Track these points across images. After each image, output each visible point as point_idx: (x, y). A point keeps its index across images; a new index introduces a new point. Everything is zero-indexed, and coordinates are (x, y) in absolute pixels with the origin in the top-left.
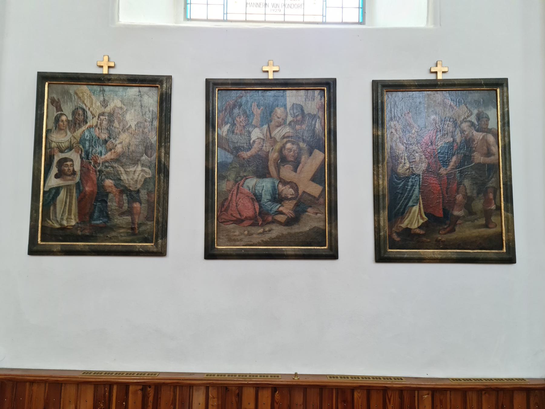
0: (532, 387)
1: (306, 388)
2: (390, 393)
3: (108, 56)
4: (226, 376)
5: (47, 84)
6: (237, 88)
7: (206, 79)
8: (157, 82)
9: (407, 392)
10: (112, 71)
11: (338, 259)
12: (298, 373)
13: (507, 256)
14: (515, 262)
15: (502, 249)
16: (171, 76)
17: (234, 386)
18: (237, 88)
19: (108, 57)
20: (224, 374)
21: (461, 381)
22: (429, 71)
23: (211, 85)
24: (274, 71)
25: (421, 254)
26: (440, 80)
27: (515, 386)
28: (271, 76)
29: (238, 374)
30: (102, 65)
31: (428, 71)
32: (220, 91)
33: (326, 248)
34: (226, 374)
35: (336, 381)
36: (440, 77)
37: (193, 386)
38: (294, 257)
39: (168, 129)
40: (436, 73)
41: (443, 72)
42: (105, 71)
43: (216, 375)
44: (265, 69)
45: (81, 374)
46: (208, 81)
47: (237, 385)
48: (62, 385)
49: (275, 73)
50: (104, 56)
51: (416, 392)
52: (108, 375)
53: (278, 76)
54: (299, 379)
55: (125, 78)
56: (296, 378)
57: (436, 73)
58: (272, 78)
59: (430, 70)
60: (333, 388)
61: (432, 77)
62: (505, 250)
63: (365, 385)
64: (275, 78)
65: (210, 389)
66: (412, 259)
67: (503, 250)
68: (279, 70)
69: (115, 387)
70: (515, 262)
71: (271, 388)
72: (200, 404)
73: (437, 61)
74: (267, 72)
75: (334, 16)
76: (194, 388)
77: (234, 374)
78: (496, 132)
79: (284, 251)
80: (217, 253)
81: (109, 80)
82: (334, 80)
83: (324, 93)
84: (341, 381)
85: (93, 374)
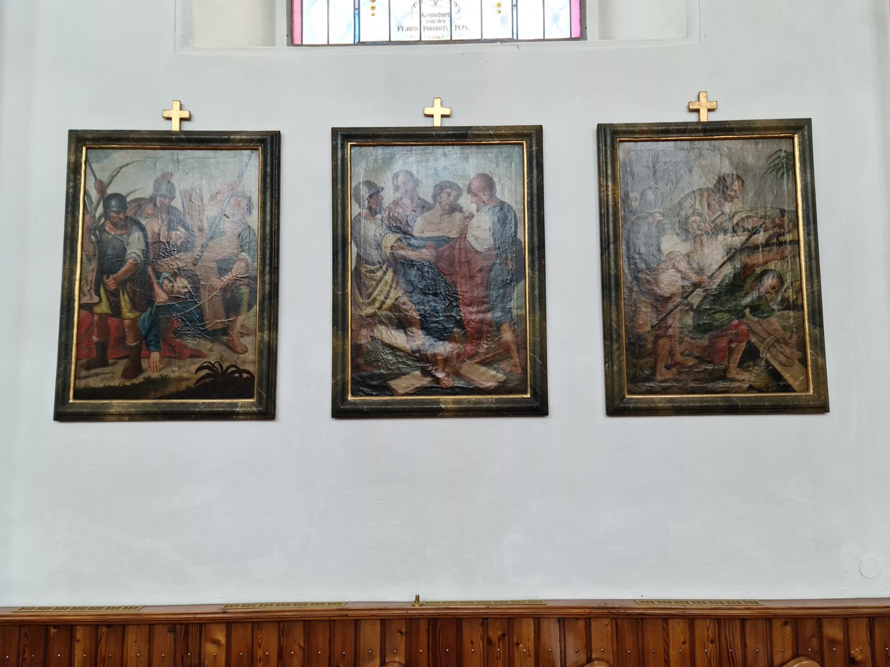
1: (590, 619)
2: (465, 626)
4: (326, 605)
5: (84, 148)
8: (467, 138)
9: (253, 626)
10: (188, 127)
11: (829, 411)
15: (808, 390)
16: (279, 132)
22: (687, 109)
25: (654, 403)
31: (685, 109)
40: (698, 111)
42: (175, 126)
44: (428, 111)
47: (574, 616)
49: (445, 119)
55: (782, 125)
57: (698, 111)
59: (689, 106)
61: (692, 118)
62: (811, 392)
71: (301, 623)
81: (227, 141)
82: (72, 133)
83: (792, 143)
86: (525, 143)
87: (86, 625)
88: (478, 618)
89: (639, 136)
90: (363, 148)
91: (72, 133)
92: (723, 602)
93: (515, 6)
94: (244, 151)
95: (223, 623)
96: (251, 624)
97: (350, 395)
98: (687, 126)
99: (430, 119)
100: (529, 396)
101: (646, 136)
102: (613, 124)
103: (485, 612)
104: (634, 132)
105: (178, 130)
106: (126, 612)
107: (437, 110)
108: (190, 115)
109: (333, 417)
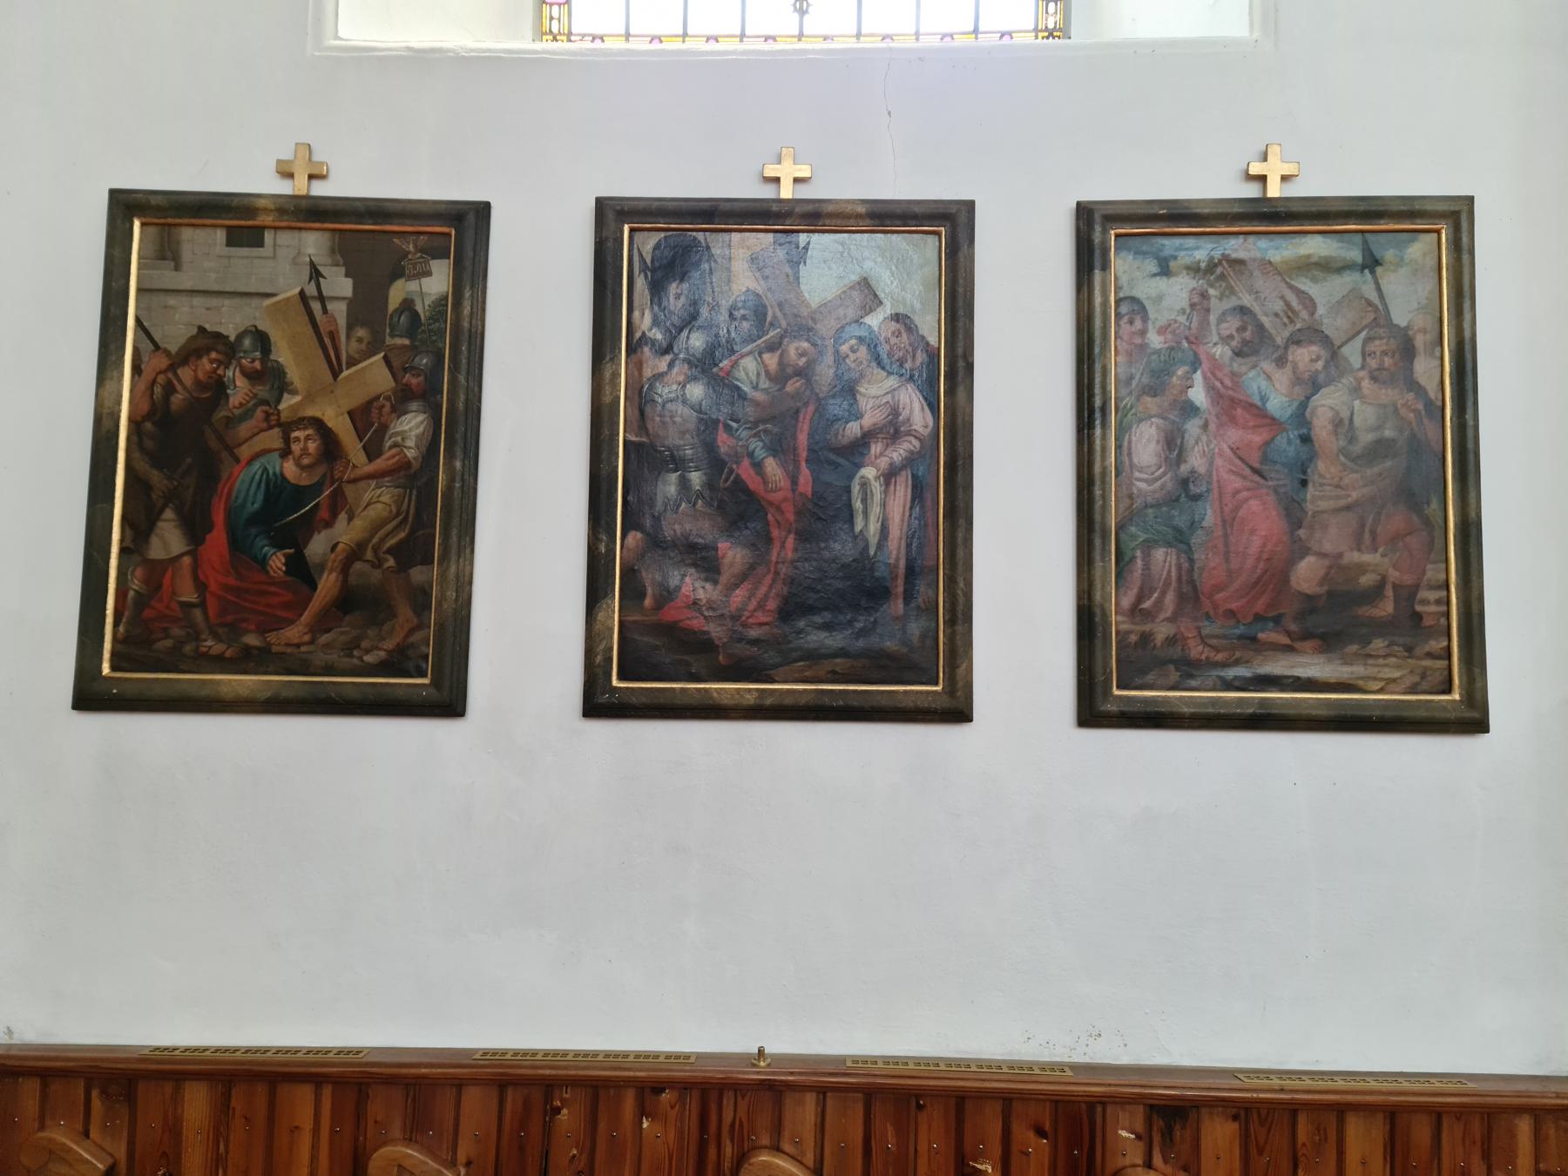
7: (596, 198)
13: (944, 702)
14: (1487, 731)
17: (1223, 1106)
21: (1336, 1083)
23: (610, 216)
26: (788, 200)
27: (871, 1080)
30: (1269, 157)
32: (1121, 240)
36: (1274, 190)
37: (1104, 1104)
40: (777, 180)
41: (797, 180)
46: (602, 205)
51: (1099, 1109)
53: (1297, 190)
54: (769, 1065)
56: (762, 1064)
58: (790, 197)
60: (1251, 1108)
62: (1457, 697)
63: (1359, 1098)
65: (1446, 1122)
68: (810, 178)
69: (1302, 1120)
70: (1487, 731)
72: (1219, 1158)
73: (1267, 145)
74: (777, 180)
75: (992, 22)
76: (1204, 1111)
77: (582, 1053)
78: (936, 352)
80: (1276, 711)
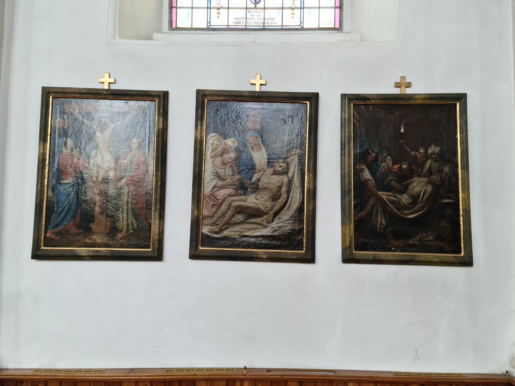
0: (7, 378)
3: (109, 73)
6: (365, 103)
9: (211, 383)
12: (247, 367)
18: (365, 103)
19: (108, 74)
20: (213, 369)
24: (261, 85)
28: (257, 89)
29: (226, 368)
33: (150, 250)
34: (224, 369)
35: (231, 374)
38: (113, 258)
39: (165, 142)
43: (195, 370)
44: (253, 81)
45: (33, 372)
48: (166, 383)
49: (262, 86)
50: (257, 74)
52: (98, 373)
55: (423, 97)
58: (399, 93)
64: (261, 91)
66: (73, 257)
67: (43, 246)
77: (222, 369)
79: (254, 254)
82: (44, 88)
84: (207, 374)
85: (74, 372)
86: (157, 101)
87: (252, 381)
88: (342, 382)
89: (146, 98)
90: (113, 101)
91: (44, 88)
92: (403, 373)
93: (302, 23)
94: (264, 103)
95: (149, 381)
96: (255, 381)
97: (200, 246)
98: (91, 91)
99: (254, 86)
100: (150, 250)
101: (231, 98)
102: (360, 94)
103: (128, 378)
104: (64, 93)
105: (108, 88)
106: (228, 373)
107: (258, 82)
108: (115, 80)
109: (189, 258)
